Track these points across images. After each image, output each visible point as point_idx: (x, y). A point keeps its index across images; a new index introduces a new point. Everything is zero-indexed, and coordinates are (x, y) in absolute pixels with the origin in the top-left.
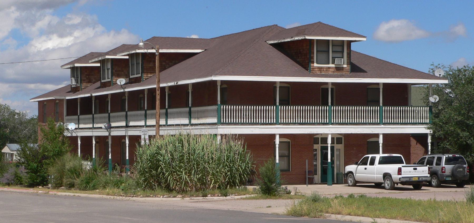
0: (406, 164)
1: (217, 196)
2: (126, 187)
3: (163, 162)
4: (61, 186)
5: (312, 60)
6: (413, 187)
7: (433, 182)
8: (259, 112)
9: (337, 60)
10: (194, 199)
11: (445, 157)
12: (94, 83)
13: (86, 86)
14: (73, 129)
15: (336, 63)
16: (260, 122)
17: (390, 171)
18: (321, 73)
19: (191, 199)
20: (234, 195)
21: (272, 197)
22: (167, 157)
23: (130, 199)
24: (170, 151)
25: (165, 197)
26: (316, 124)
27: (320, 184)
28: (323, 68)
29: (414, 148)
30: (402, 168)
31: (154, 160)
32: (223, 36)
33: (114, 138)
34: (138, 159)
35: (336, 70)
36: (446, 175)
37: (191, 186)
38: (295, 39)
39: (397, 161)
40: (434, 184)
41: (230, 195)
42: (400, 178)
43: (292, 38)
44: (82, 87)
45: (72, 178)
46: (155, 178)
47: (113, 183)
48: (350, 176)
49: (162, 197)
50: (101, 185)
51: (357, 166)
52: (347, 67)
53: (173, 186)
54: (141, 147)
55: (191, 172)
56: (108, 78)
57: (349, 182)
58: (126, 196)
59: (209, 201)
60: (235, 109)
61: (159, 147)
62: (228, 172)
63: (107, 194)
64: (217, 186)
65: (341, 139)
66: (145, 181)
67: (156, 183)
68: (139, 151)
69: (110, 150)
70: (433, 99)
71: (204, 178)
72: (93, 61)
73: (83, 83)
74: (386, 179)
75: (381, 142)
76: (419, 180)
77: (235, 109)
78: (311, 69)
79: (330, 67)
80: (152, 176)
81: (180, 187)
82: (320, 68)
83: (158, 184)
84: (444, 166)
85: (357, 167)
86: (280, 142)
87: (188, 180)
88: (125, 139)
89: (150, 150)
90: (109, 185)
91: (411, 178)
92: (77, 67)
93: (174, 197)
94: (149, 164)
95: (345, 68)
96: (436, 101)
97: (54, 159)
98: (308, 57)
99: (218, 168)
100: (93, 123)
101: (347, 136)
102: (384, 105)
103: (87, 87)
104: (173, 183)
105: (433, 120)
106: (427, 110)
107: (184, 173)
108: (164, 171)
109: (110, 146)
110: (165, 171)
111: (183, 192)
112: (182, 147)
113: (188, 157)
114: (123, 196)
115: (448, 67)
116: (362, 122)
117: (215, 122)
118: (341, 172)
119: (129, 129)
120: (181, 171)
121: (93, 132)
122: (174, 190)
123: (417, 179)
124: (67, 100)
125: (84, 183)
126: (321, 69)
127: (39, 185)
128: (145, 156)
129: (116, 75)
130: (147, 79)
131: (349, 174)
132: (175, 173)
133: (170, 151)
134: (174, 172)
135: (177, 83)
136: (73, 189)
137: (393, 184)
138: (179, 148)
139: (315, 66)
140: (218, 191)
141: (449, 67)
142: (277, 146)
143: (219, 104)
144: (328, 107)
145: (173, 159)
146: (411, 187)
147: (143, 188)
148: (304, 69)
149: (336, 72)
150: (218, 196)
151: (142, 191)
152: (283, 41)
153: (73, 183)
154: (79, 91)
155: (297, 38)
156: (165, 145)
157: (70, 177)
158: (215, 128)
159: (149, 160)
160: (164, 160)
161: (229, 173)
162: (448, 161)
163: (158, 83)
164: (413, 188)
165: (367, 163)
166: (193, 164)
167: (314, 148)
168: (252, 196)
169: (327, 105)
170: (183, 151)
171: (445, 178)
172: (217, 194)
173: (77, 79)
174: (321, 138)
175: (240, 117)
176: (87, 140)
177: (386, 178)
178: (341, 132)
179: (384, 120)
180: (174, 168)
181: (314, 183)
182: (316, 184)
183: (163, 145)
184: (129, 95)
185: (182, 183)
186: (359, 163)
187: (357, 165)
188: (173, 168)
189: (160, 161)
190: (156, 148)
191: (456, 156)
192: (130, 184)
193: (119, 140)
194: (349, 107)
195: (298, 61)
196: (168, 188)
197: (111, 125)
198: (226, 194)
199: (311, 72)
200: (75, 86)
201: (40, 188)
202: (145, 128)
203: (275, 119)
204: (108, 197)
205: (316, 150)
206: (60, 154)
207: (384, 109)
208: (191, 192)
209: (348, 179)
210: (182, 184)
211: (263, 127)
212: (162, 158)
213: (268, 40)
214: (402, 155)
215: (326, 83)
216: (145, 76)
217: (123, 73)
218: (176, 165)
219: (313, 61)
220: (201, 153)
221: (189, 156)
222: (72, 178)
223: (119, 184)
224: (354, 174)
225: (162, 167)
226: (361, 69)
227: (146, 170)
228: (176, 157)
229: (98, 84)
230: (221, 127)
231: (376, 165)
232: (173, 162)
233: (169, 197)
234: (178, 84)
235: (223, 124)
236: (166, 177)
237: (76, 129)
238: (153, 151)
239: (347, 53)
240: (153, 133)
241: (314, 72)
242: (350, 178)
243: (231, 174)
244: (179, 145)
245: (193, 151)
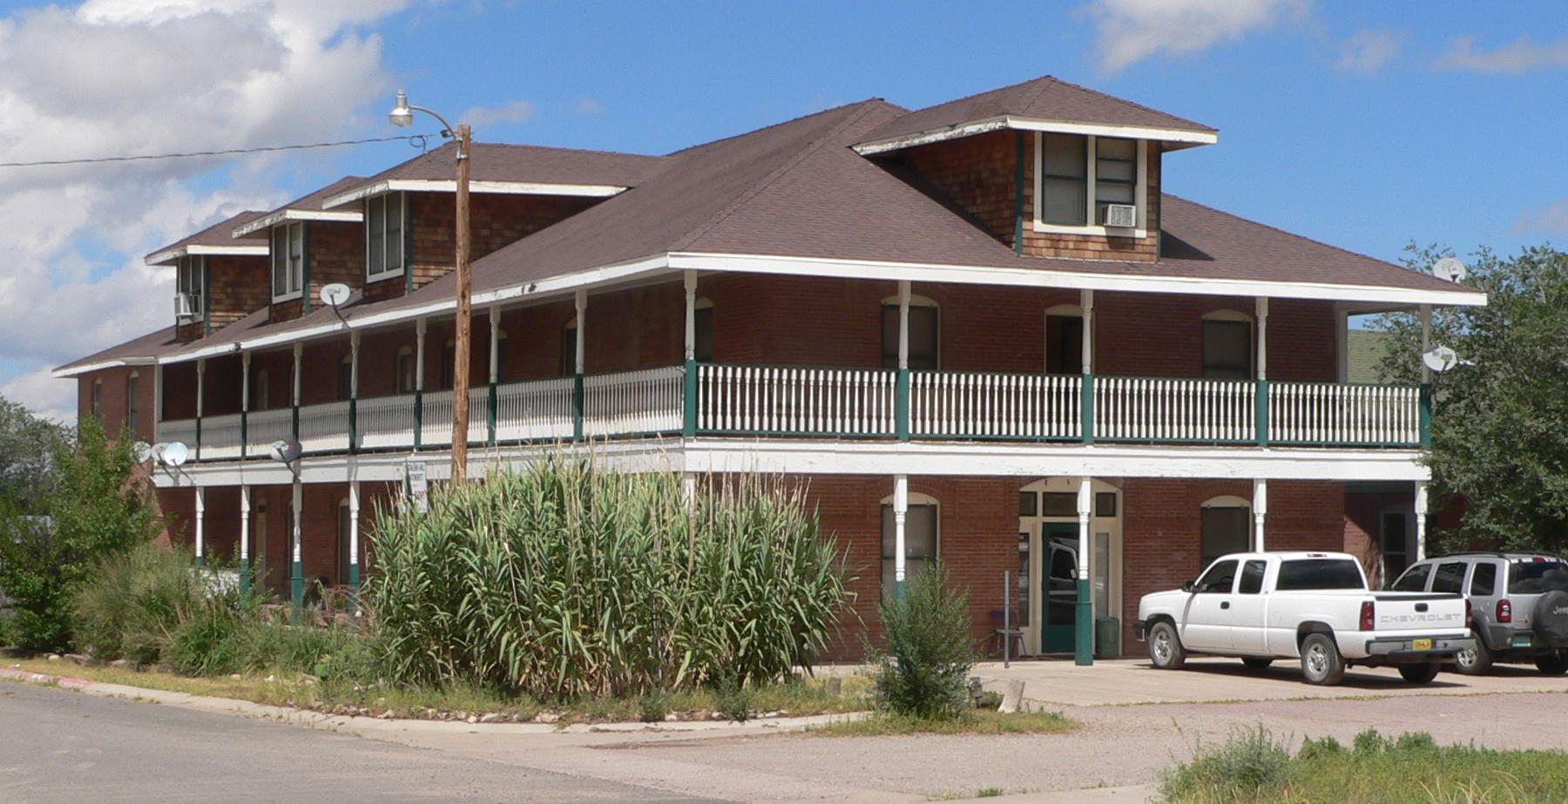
1: (702, 717)
2: (336, 670)
3: (478, 576)
4: (116, 658)
5: (1026, 208)
6: (1402, 674)
9: (1113, 211)
10: (607, 731)
11: (1507, 564)
12: (250, 312)
13: (224, 319)
14: (180, 461)
16: (838, 430)
18: (1056, 255)
19: (597, 730)
20: (774, 714)
21: (936, 725)
22: (498, 552)
23: (343, 723)
24: (510, 532)
25: (486, 721)
27: (1040, 658)
28: (1063, 238)
30: (1378, 605)
31: (443, 569)
32: (687, 149)
33: (309, 489)
34: (378, 564)
36: (1513, 629)
37: (595, 672)
38: (963, 132)
39: (1342, 578)
40: (1464, 662)
41: (760, 716)
42: (1368, 643)
43: (953, 127)
44: (212, 325)
45: (152, 627)
46: (445, 639)
47: (292, 651)
48: (1163, 629)
49: (473, 719)
50: (248, 658)
51: (1190, 594)
53: (520, 675)
54: (390, 514)
55: (593, 616)
56: (294, 290)
57: (1158, 653)
58: (331, 712)
59: (677, 744)
61: (463, 513)
62: (750, 620)
63: (257, 699)
64: (702, 676)
65: (1111, 498)
66: (405, 650)
67: (451, 661)
68: (386, 528)
69: (297, 531)
70: (1437, 360)
71: (647, 642)
72: (245, 231)
73: (214, 311)
76: (1434, 650)
80: (436, 633)
81: (550, 680)
82: (1055, 237)
83: (457, 662)
84: (1505, 595)
85: (1191, 598)
86: (910, 506)
87: (584, 650)
88: (348, 496)
89: (426, 526)
90: (278, 657)
91: (1407, 643)
92: (196, 257)
93: (526, 720)
94: (422, 581)
95: (1142, 242)
96: (1448, 368)
97: (98, 562)
98: (1013, 196)
99: (707, 600)
100: (244, 442)
101: (1135, 486)
102: (1273, 376)
103: (228, 323)
104: (522, 665)
106: (1413, 398)
107: (566, 621)
108: (485, 613)
109: (297, 517)
110: (489, 611)
111: (560, 698)
112: (561, 511)
113: (585, 556)
114: (319, 709)
115: (1477, 253)
116: (1175, 436)
117: (675, 428)
118: (1110, 615)
119: (359, 461)
120: (554, 612)
121: (244, 473)
122: (525, 689)
123: (1426, 646)
124: (166, 367)
125: (190, 648)
126: (1058, 241)
127: (51, 650)
128: (407, 552)
129: (321, 276)
130: (426, 284)
131: (1153, 625)
132: (530, 622)
133: (510, 532)
134: (525, 618)
135: (533, 288)
136: (153, 668)
137: (1338, 664)
138: (547, 519)
140: (708, 698)
141: (1481, 250)
142: (900, 519)
143: (692, 358)
144: (1080, 380)
145: (521, 563)
146: (1394, 673)
147: (397, 676)
148: (998, 244)
149: (1108, 255)
150: (709, 718)
151: (395, 693)
152: (916, 142)
153: (155, 648)
154: (200, 336)
155: (971, 129)
156: (489, 504)
157: (145, 627)
158: (674, 450)
159: (425, 566)
160: (485, 568)
161: (753, 623)
162: (1523, 578)
163: (465, 270)
164: (1400, 676)
165: (1231, 584)
166: (606, 584)
167: (1021, 531)
168: (851, 720)
169: (1076, 371)
170: (564, 530)
171: (1509, 640)
172: (704, 711)
173: (196, 298)
174: (1044, 494)
176: (223, 500)
177: (1309, 638)
178: (1124, 471)
179: (1271, 429)
180: (527, 601)
181: (1021, 652)
182: (1025, 658)
183: (480, 505)
184: (361, 342)
185: (560, 661)
186: (1196, 583)
187: (1189, 591)
188: (521, 601)
189: (468, 572)
190: (453, 519)
192: (353, 657)
193: (328, 498)
194: (1152, 383)
195: (973, 214)
196: (499, 680)
197: (300, 447)
198: (743, 710)
199: (1025, 250)
200: (188, 322)
201: (49, 662)
202: (416, 454)
203: (892, 422)
204: (260, 710)
205: (1026, 535)
206: (118, 543)
207: (1271, 391)
208: (594, 699)
209: (1150, 642)
210: (558, 666)
211: (850, 450)
212: (476, 559)
213: (859, 144)
214: (1357, 557)
215: (1073, 296)
216: (420, 273)
217: (343, 271)
218: (535, 590)
219: (1030, 210)
220: (637, 538)
221: (588, 552)
222: (150, 630)
223: (313, 655)
224: (1179, 626)
225: (476, 596)
227: (408, 605)
228: (535, 555)
229: (263, 314)
230: (695, 444)
231: (1266, 593)
232: (522, 573)
233: (505, 720)
234: (536, 291)
235: (704, 434)
236: (491, 638)
237: (188, 462)
238: (440, 529)
239: (1148, 186)
240: (442, 471)
241: (1033, 251)
242: (1158, 639)
243: (759, 627)
244: (548, 503)
245: (602, 530)
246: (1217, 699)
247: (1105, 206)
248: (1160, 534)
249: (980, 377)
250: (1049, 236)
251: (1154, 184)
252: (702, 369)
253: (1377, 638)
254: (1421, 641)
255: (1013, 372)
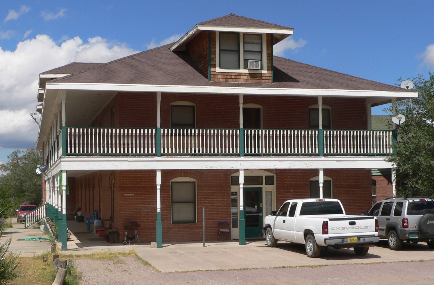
0: (347, 214)
7: (390, 241)
8: (291, 140)
11: (407, 202)
15: (250, 68)
17: (312, 227)
26: (220, 155)
28: (229, 74)
29: (385, 189)
30: (330, 222)
35: (251, 78)
36: (409, 230)
52: (267, 73)
60: (253, 135)
65: (261, 178)
74: (308, 241)
75: (321, 182)
77: (253, 135)
78: (211, 75)
79: (241, 73)
82: (225, 74)
85: (276, 218)
95: (265, 75)
105: (396, 148)
139: (216, 71)
144: (238, 131)
171: (407, 235)
174: (266, 176)
175: (342, 146)
177: (308, 236)
179: (325, 149)
191: (425, 200)
211: (196, 160)
214: (339, 200)
219: (215, 64)
226: (289, 76)
246: (235, 268)
247: (247, 61)
248: (292, 191)
249: (345, 132)
250: (223, 74)
251: (270, 52)
252: (325, 132)
253: (329, 237)
254: (353, 238)
255: (345, 129)
